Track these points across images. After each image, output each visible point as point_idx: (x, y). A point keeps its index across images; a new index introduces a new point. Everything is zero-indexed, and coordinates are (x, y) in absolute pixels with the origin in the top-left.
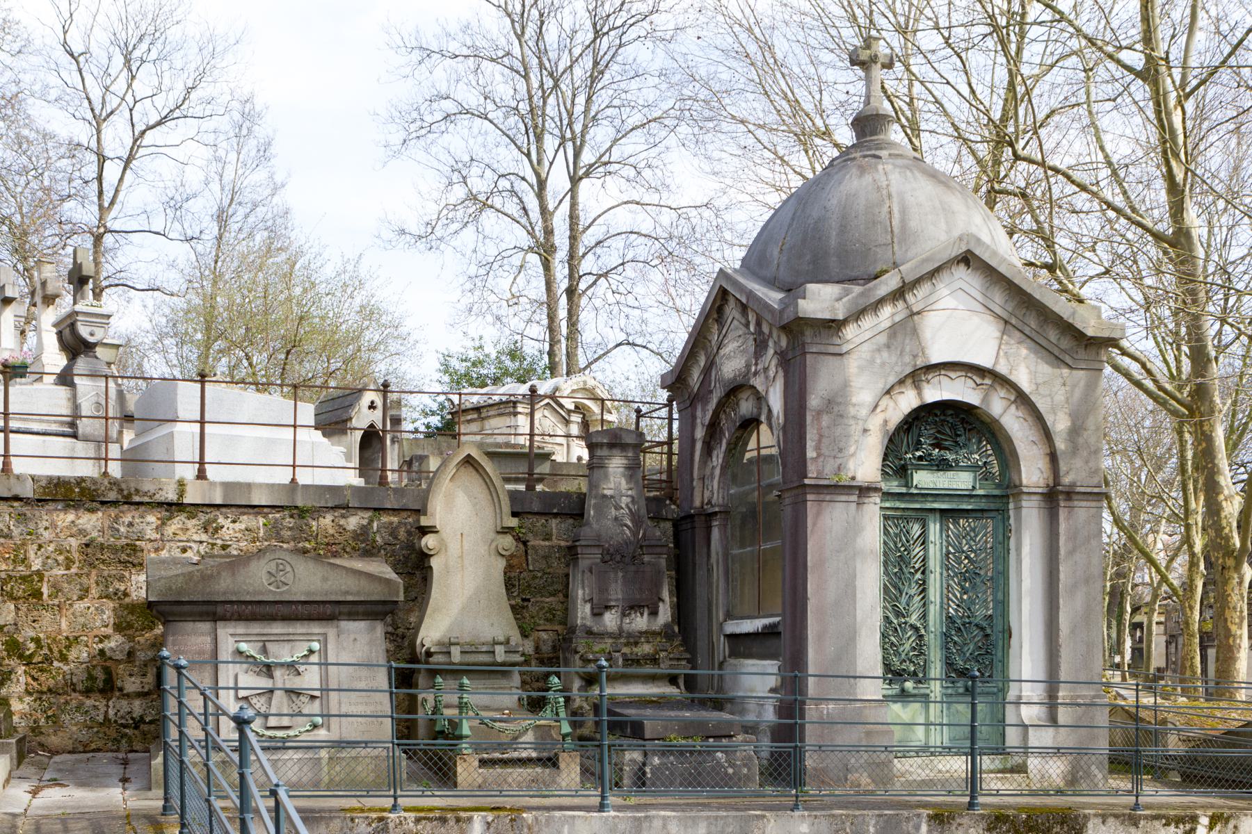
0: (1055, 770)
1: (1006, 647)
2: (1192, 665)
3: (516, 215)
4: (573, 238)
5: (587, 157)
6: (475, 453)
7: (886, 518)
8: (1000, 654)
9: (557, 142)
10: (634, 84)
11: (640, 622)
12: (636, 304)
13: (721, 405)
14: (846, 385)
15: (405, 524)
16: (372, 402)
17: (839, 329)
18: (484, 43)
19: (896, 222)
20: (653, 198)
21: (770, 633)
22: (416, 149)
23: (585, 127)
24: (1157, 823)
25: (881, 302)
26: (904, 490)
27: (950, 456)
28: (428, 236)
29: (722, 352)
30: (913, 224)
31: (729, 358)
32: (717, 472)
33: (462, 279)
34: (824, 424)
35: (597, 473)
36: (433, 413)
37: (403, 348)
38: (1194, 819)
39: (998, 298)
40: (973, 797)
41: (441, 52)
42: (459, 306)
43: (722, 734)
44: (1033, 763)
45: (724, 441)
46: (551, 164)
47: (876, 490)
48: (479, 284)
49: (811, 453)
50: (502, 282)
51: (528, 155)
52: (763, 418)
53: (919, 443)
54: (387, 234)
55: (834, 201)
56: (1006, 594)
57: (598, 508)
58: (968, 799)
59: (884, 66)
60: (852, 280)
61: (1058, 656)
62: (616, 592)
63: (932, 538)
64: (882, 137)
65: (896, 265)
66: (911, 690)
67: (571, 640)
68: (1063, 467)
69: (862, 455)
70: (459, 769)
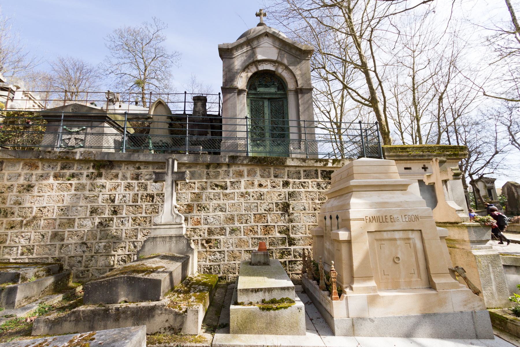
39: (277, 44)
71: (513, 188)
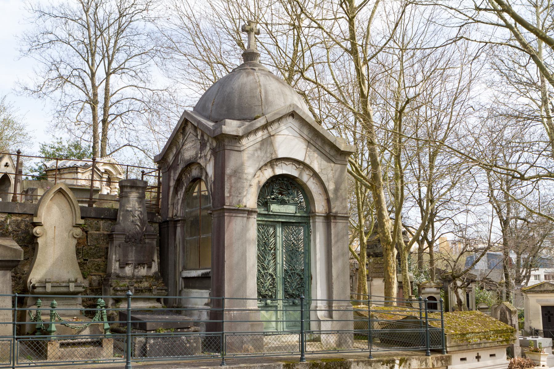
0: (332, 340)
1: (310, 284)
2: (364, 289)
3: (80, 87)
4: (106, 99)
5: (114, 65)
6: (63, 188)
7: (259, 225)
8: (307, 287)
9: (101, 57)
10: (136, 38)
11: (143, 271)
12: (134, 129)
13: (183, 171)
14: (242, 164)
15: (25, 221)
16: (7, 163)
17: (240, 140)
18: (70, 13)
19: (263, 97)
20: (141, 85)
21: (205, 277)
22: (35, 54)
23: (114, 52)
24: (379, 364)
25: (258, 129)
26: (266, 213)
27: (286, 199)
28: (38, 92)
29: (184, 147)
30: (270, 98)
31: (187, 150)
32: (180, 201)
33: (53, 112)
34: (233, 181)
35: (124, 200)
36: (36, 171)
37: (24, 140)
38: (393, 361)
39: (305, 132)
40: (302, 355)
41: (49, 14)
42: (51, 123)
43: (184, 327)
44: (323, 337)
45: (184, 188)
46: (98, 66)
47: (255, 212)
48: (62, 114)
49: (227, 194)
50: (73, 114)
51: (88, 62)
52: (203, 178)
53: (273, 192)
54: (18, 89)
55: (236, 86)
56: (310, 260)
57: (124, 216)
58: (300, 356)
59: (256, 33)
60: (244, 119)
61: (332, 288)
62: (132, 257)
63: (278, 234)
64: (255, 62)
65: (263, 115)
66: (270, 304)
67: (108, 280)
68: (332, 205)
69: (249, 196)
70: (49, 348)
71: (507, 313)
